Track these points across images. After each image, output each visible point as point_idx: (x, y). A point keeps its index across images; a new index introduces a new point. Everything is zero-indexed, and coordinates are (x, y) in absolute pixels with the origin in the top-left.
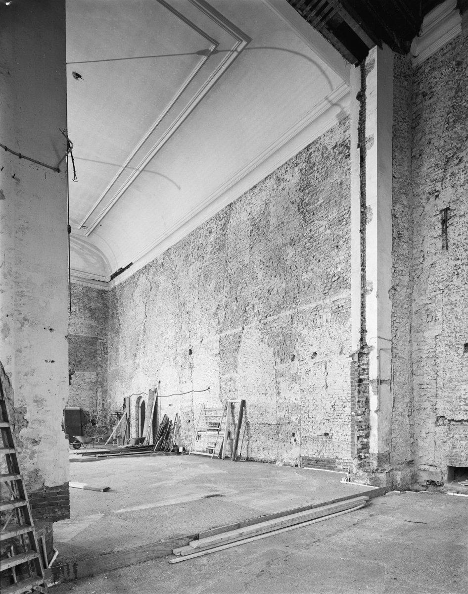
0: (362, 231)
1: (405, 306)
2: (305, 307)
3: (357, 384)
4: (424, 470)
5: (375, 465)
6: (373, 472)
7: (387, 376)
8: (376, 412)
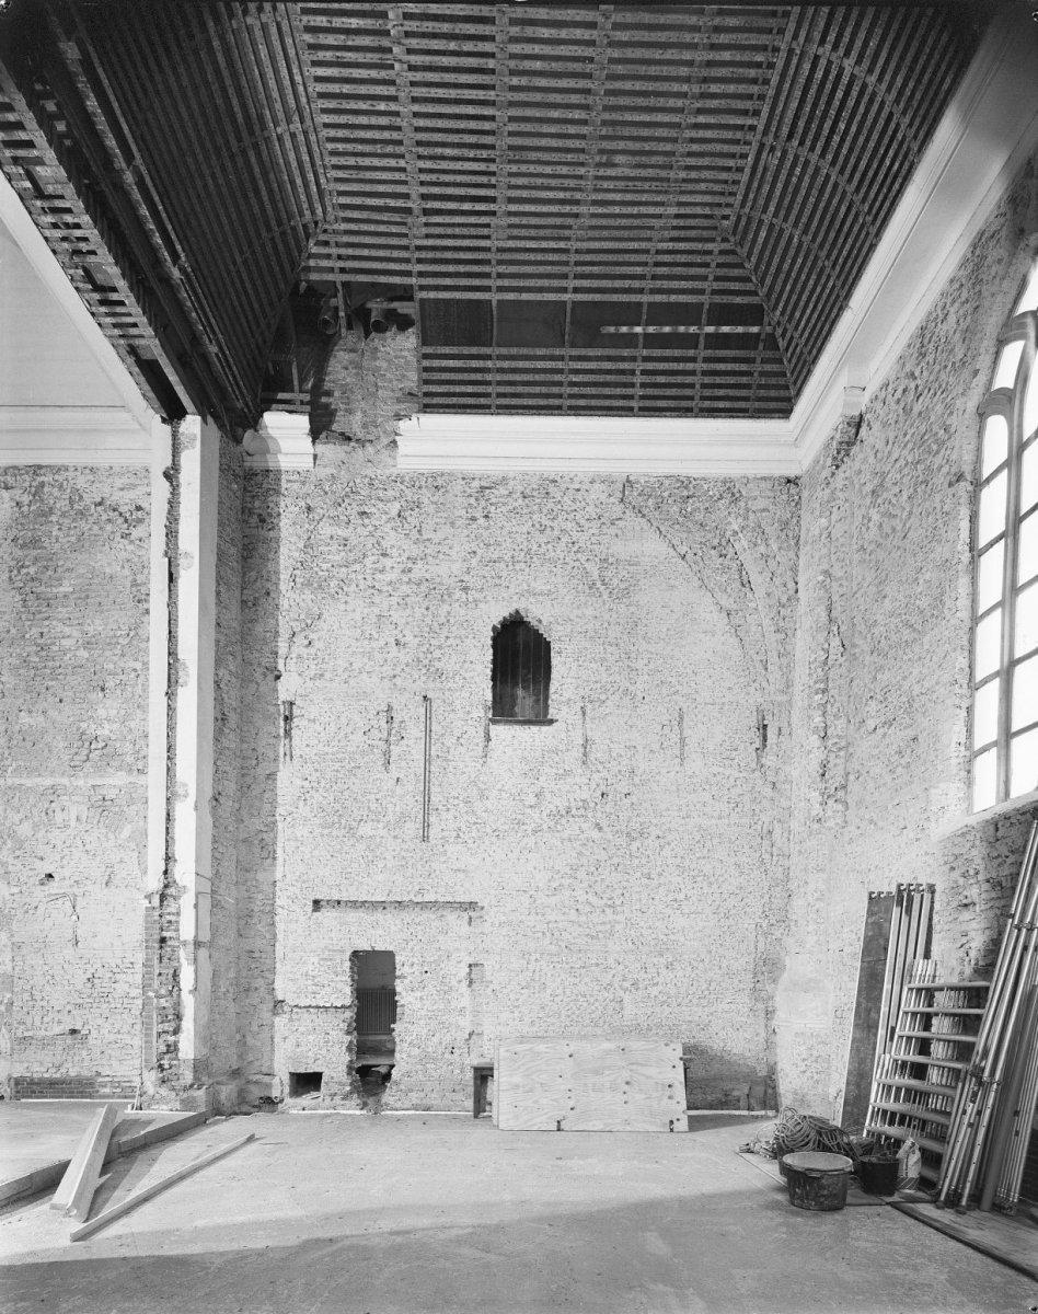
0: (170, 695)
1: (230, 828)
3: (157, 945)
4: (256, 1082)
5: (188, 1077)
6: (185, 1089)
7: (205, 936)
8: (190, 992)
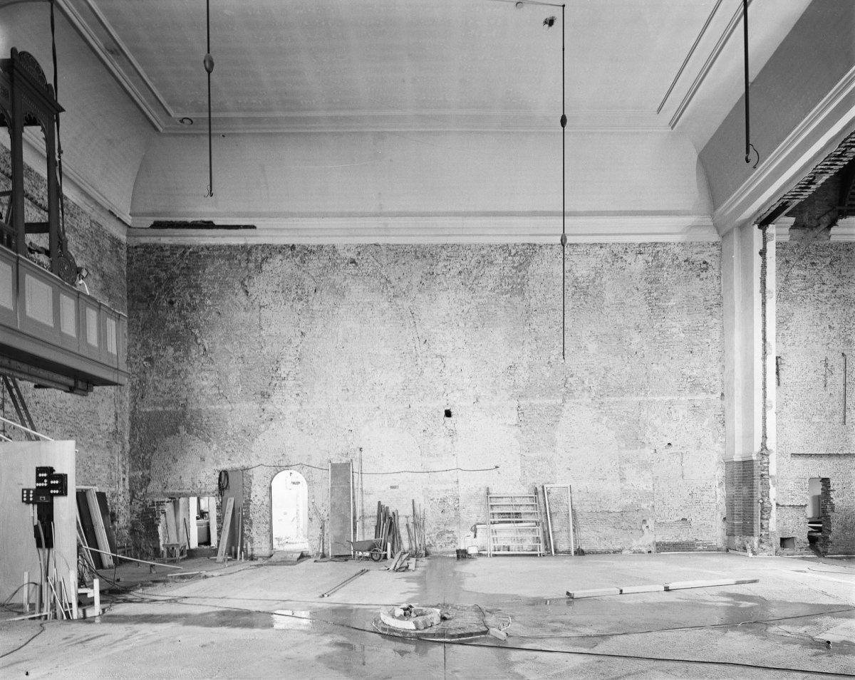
2: (658, 399)
